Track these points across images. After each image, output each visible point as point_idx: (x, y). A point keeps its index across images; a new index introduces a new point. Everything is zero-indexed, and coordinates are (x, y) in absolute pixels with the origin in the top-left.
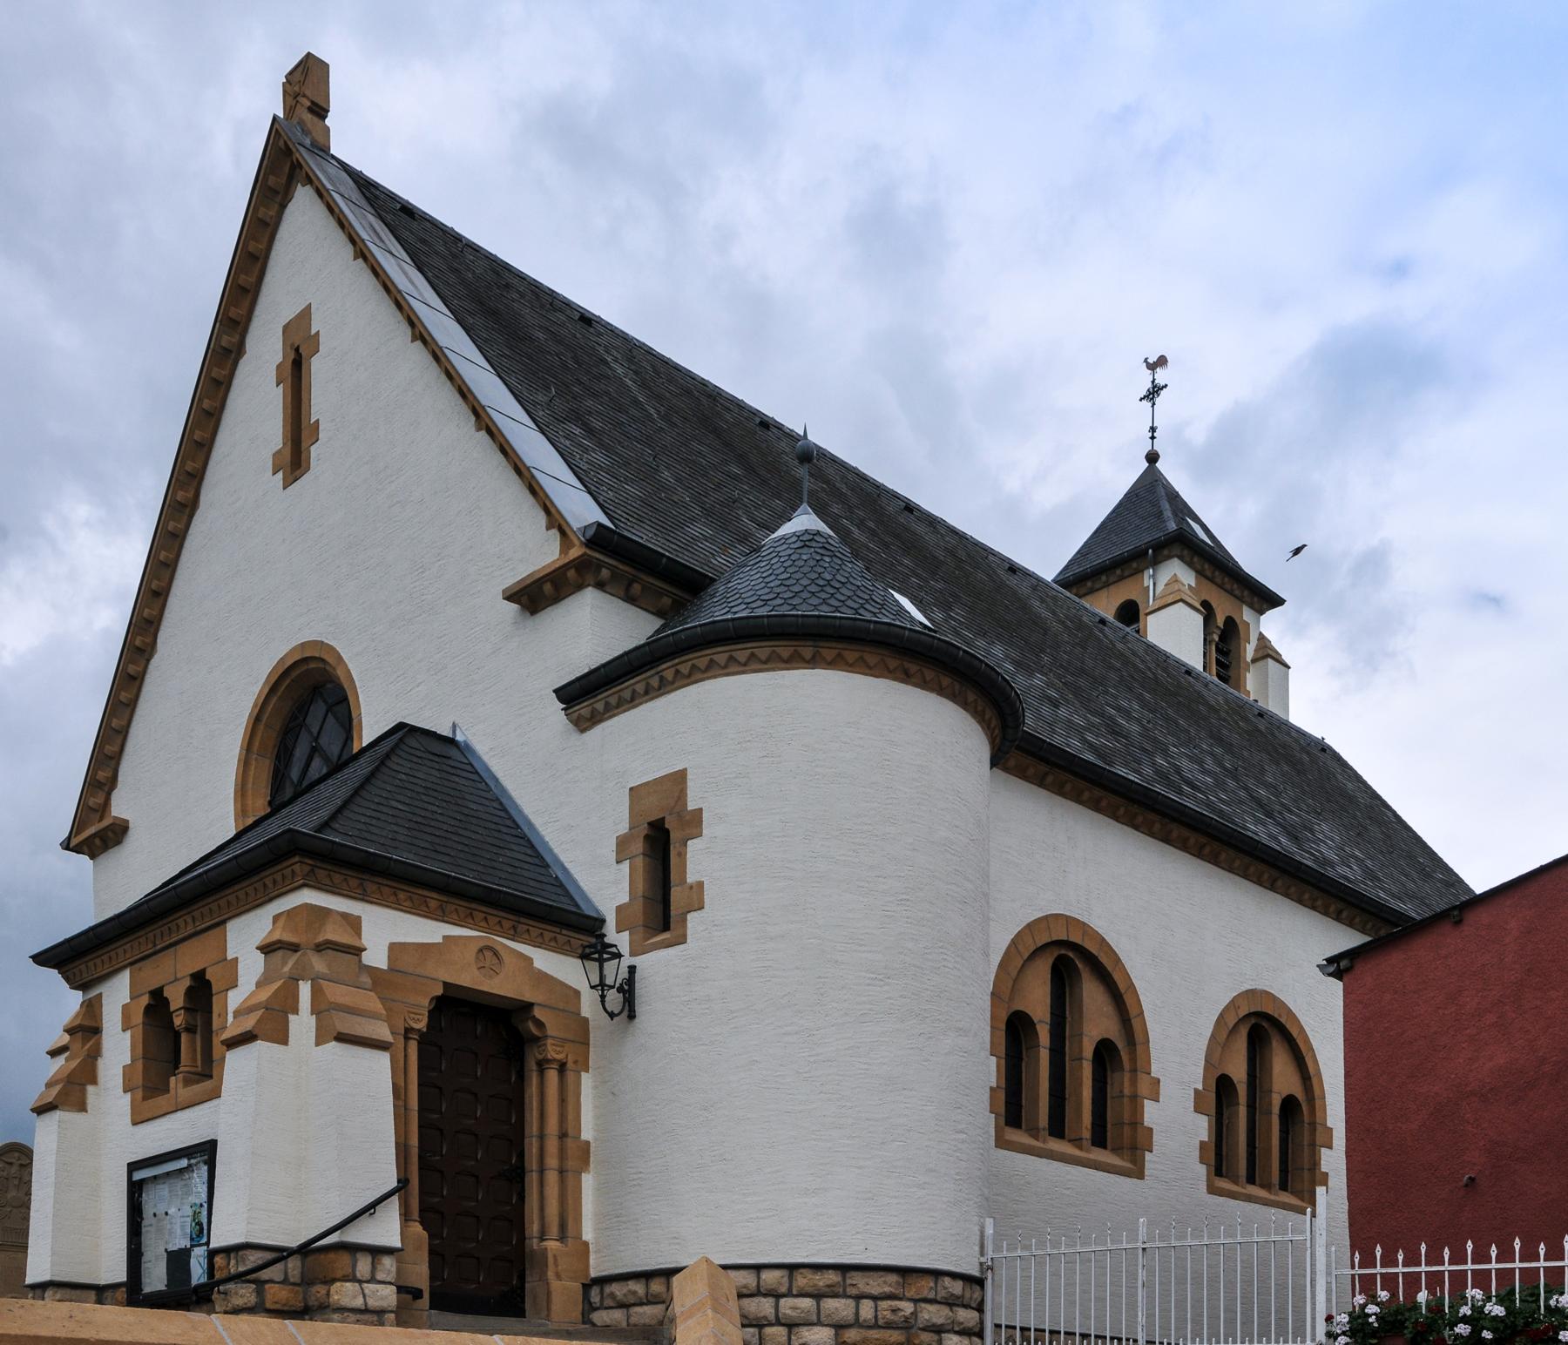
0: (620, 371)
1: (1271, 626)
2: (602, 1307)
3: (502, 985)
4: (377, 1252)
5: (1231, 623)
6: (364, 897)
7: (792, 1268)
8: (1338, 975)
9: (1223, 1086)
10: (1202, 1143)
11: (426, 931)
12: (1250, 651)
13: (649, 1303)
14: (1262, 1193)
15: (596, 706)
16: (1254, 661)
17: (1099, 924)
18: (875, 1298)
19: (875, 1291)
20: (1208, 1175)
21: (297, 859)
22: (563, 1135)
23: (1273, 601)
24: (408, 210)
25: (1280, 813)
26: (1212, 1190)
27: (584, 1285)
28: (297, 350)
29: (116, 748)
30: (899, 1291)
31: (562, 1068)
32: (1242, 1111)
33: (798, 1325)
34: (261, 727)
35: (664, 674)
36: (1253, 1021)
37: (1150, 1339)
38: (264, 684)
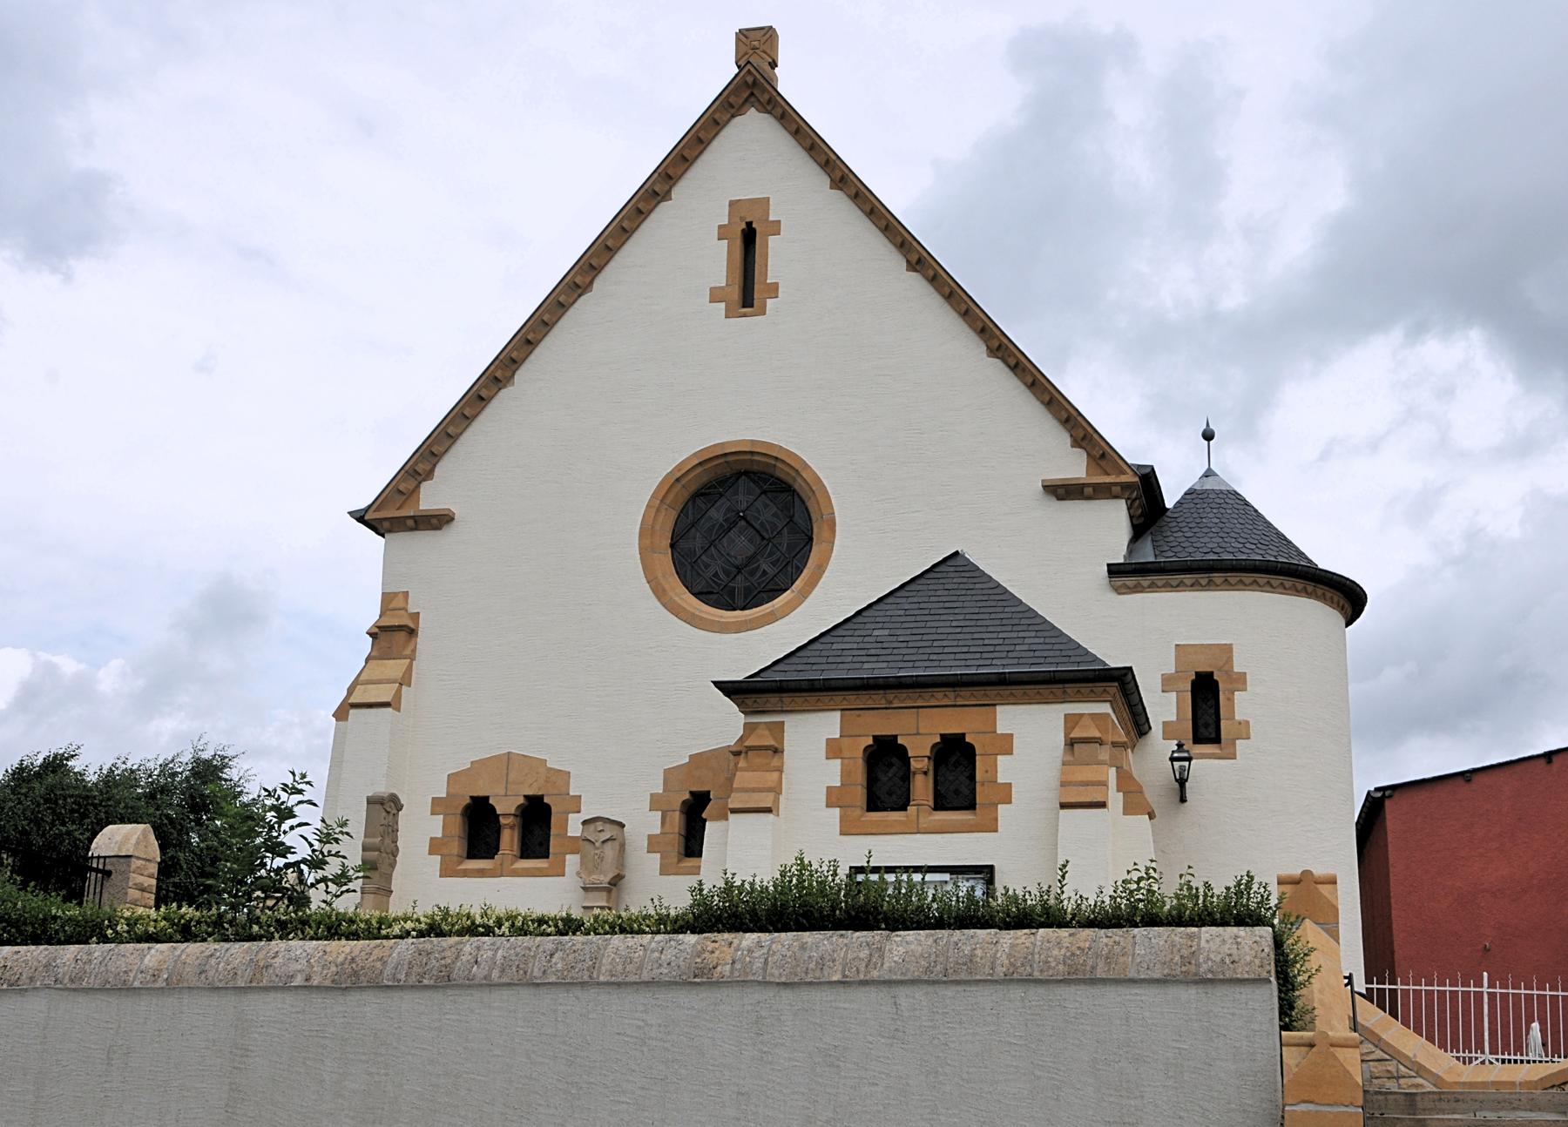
29: (442, 449)
34: (679, 486)
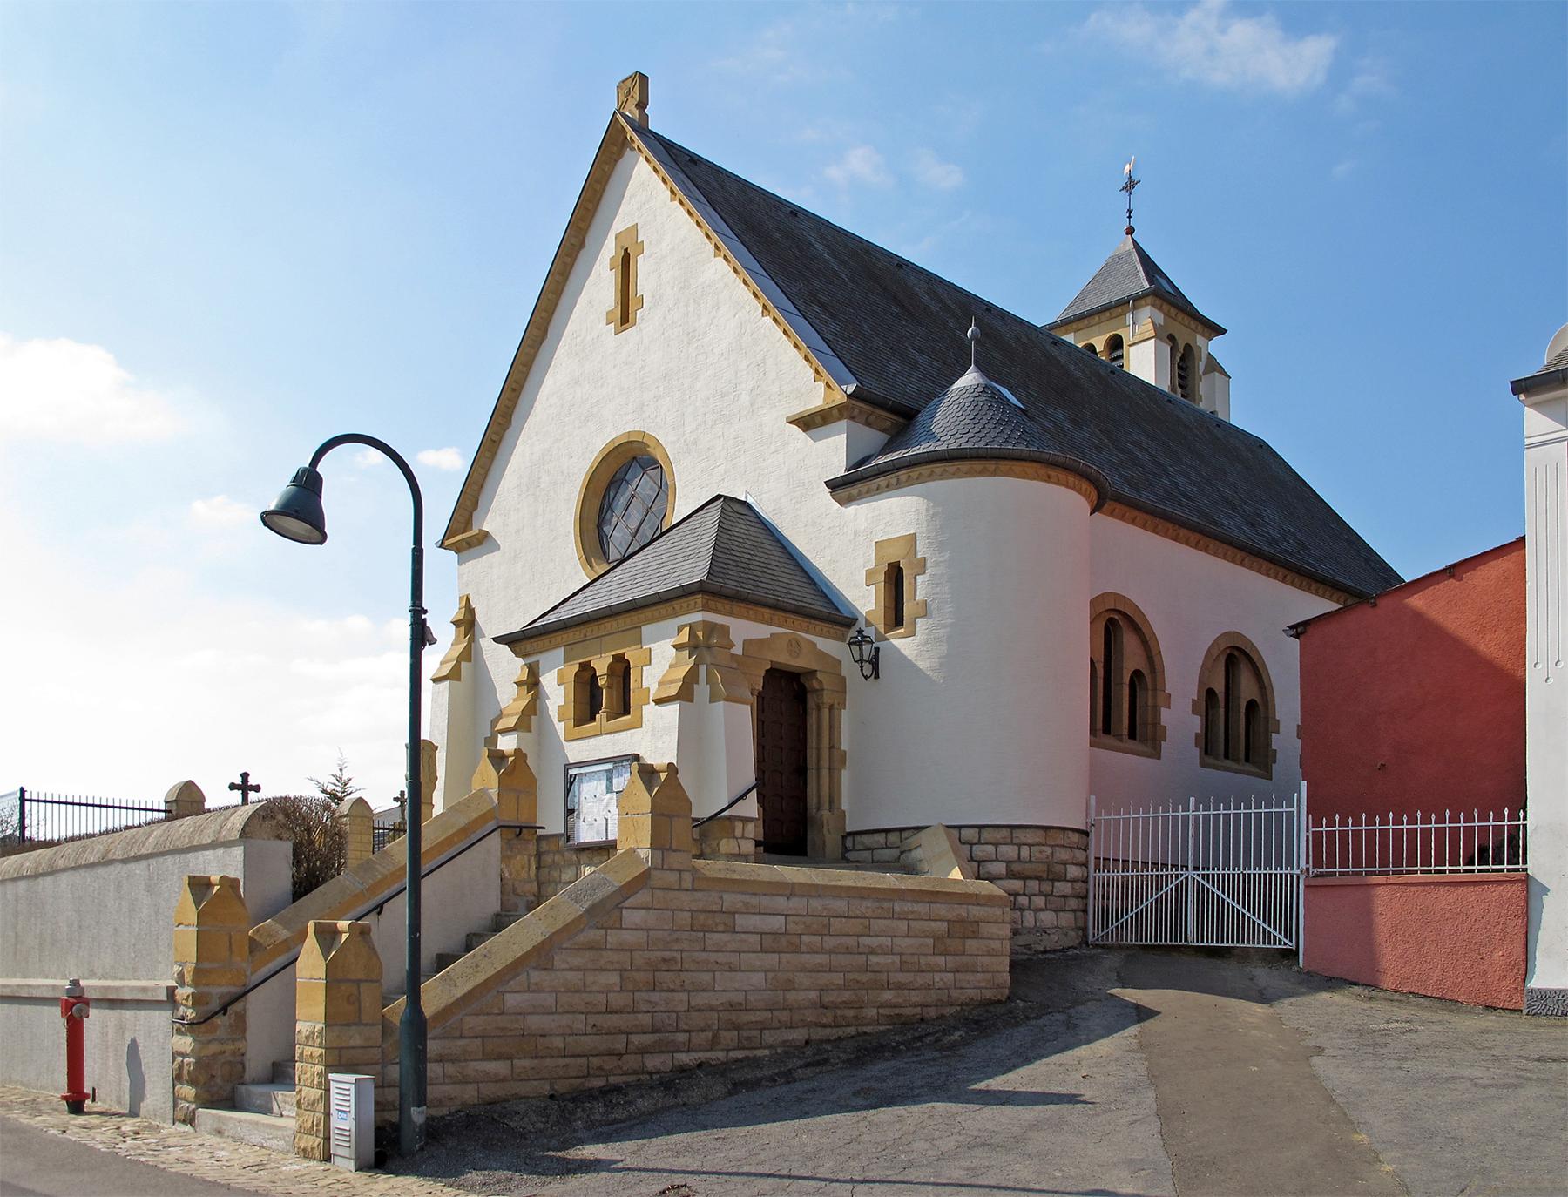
0: (820, 248)
1: (1215, 347)
2: (854, 849)
3: (801, 662)
4: (745, 820)
5: (1188, 347)
6: (731, 614)
7: (981, 827)
8: (1297, 636)
9: (1211, 694)
10: (1196, 734)
11: (762, 631)
12: (1201, 366)
13: (887, 847)
14: (1235, 765)
15: (852, 492)
16: (1204, 373)
17: (1133, 596)
18: (1030, 845)
19: (1030, 841)
20: (1200, 755)
21: (700, 596)
22: (831, 747)
23: (1217, 330)
24: (694, 160)
25: (1241, 507)
26: (1203, 764)
27: (843, 837)
28: (626, 250)
30: (1043, 842)
31: (831, 707)
32: (1222, 711)
33: (984, 861)
35: (901, 477)
36: (1229, 652)
37: (1097, 856)
38: (598, 455)
